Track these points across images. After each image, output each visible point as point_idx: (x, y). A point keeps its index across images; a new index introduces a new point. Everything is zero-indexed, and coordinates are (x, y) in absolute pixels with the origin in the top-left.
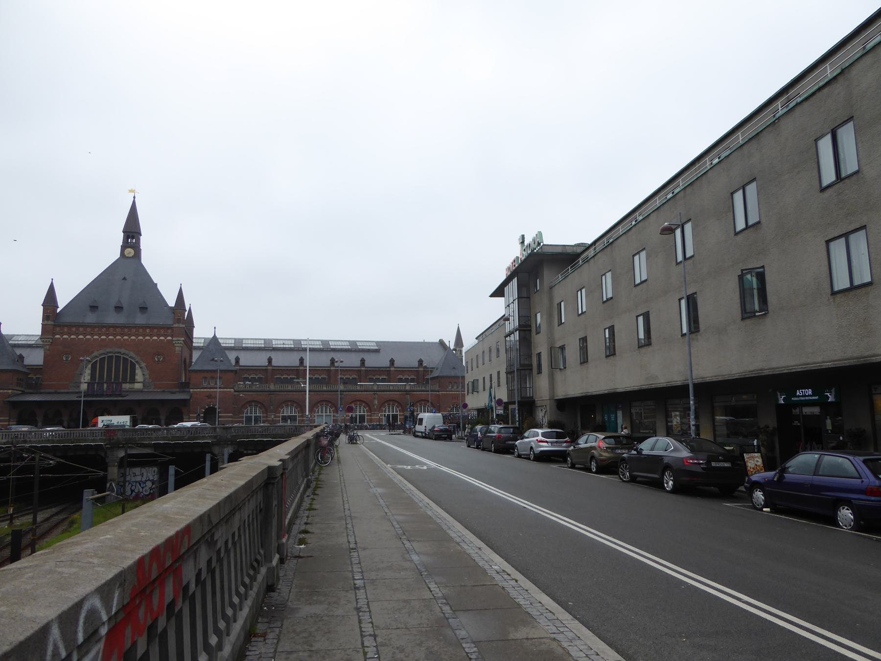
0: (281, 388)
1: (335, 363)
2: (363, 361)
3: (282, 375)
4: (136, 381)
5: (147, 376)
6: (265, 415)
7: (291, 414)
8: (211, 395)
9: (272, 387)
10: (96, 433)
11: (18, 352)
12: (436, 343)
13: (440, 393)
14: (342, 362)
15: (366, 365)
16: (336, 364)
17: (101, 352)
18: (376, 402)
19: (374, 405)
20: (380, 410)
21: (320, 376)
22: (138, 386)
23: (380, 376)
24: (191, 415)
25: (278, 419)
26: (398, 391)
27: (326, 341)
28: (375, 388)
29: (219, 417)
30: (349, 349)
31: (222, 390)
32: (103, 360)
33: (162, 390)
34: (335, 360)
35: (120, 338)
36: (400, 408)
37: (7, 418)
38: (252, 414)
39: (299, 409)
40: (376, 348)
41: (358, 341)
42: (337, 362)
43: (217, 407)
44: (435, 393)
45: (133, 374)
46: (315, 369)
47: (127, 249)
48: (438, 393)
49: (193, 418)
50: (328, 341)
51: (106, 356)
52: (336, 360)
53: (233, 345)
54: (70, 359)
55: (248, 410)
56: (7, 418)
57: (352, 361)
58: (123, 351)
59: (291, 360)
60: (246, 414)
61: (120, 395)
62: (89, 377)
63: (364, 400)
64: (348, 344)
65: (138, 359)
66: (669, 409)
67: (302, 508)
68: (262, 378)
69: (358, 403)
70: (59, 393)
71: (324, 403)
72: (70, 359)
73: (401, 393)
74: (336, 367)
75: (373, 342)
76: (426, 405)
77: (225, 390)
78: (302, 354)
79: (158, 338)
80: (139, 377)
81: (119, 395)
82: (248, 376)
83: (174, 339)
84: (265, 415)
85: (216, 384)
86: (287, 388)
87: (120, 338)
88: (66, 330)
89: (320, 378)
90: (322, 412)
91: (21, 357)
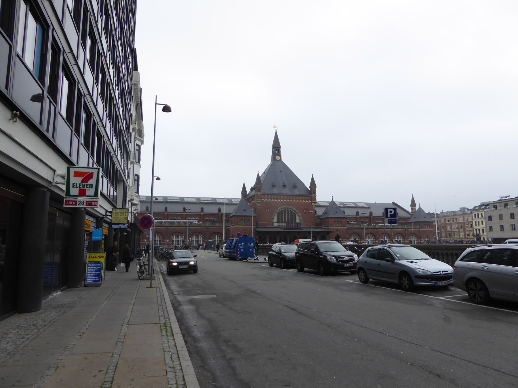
1: (186, 211)
2: (202, 210)
5: (302, 220)
9: (406, 227)
11: (342, 210)
12: (390, 204)
13: (420, 230)
14: (190, 210)
15: (204, 212)
16: (186, 211)
17: (282, 207)
23: (379, 221)
26: (401, 229)
27: (214, 198)
28: (391, 227)
30: (195, 202)
34: (185, 208)
35: (276, 200)
36: (374, 237)
38: (177, 240)
41: (217, 198)
42: (187, 209)
44: (418, 230)
46: (212, 215)
48: (419, 230)
50: (167, 197)
51: (280, 211)
52: (187, 208)
53: (145, 200)
54: (268, 211)
58: (291, 207)
59: (214, 210)
61: (300, 229)
62: (277, 220)
64: (195, 199)
65: (297, 211)
69: (214, 235)
70: (266, 227)
72: (268, 211)
73: (403, 229)
74: (186, 213)
75: (210, 198)
78: (219, 206)
79: (284, 200)
83: (313, 202)
88: (266, 197)
89: (209, 219)
90: (176, 239)
91: (344, 212)
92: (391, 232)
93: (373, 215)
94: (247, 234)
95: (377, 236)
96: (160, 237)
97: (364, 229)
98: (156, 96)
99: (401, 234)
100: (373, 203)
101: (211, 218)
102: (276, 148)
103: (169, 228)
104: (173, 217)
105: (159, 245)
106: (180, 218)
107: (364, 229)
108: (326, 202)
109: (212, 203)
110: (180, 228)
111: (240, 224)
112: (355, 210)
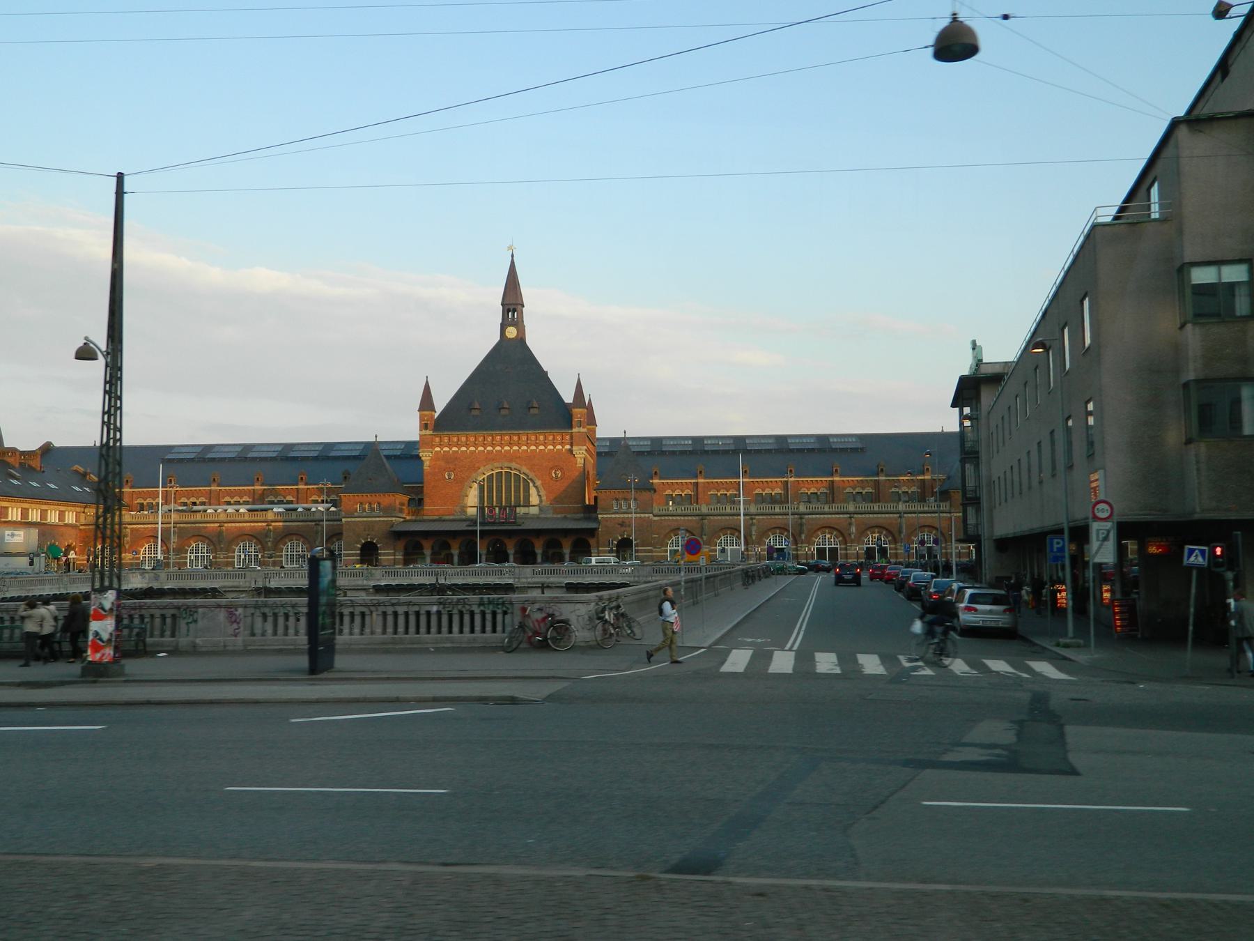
0: (837, 509)
4: (531, 504)
5: (544, 498)
6: (843, 546)
7: (781, 547)
8: (623, 522)
18: (853, 529)
19: (850, 535)
20: (859, 540)
21: (154, 500)
22: (534, 511)
24: (600, 549)
29: (637, 551)
31: (638, 515)
32: (491, 477)
33: (563, 515)
37: (392, 551)
40: (859, 445)
43: (633, 537)
45: (527, 496)
47: (509, 328)
48: (948, 515)
49: (605, 552)
55: (721, 540)
56: (392, 551)
60: (817, 545)
61: (514, 523)
63: (836, 527)
66: (358, 552)
69: (729, 532)
71: (778, 531)
76: (931, 533)
77: (642, 515)
80: (534, 499)
81: (514, 523)
84: (843, 546)
85: (629, 507)
86: (216, 519)
87: (517, 448)
92: (850, 524)
94: (361, 541)
95: (800, 536)
96: (836, 540)
98: (120, 177)
99: (887, 529)
102: (512, 303)
104: (232, 498)
108: (121, 458)
109: (820, 451)
111: (356, 514)
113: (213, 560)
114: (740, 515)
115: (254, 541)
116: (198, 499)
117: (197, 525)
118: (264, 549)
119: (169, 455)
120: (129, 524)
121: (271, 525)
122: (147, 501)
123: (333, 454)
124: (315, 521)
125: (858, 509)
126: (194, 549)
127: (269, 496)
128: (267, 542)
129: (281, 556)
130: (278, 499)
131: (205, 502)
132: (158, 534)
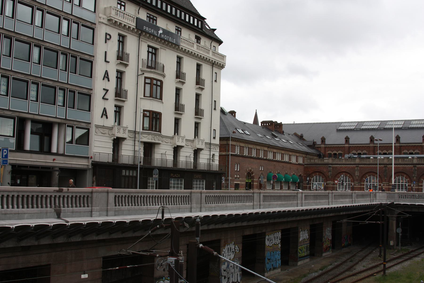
3: (332, 151)
10: (409, 195)
15: (350, 142)
16: (375, 142)
25: (363, 186)
34: (374, 138)
39: (408, 179)
55: (314, 178)
57: (339, 139)
67: (404, 260)
68: (342, 153)
82: (331, 152)
86: (382, 162)
93: (327, 142)
97: (378, 166)
98: (106, 52)
100: (290, 124)
101: (335, 152)
103: (388, 166)
104: (408, 150)
105: (404, 191)
106: (418, 152)
107: (378, 166)
110: (403, 166)
112: (344, 135)
113: (326, 186)
114: (392, 164)
115: (405, 176)
116: (357, 151)
117: (370, 166)
118: (411, 181)
119: (363, 126)
120: (331, 164)
121: (416, 167)
122: (334, 152)
123: (363, 127)
124: (384, 164)
125: (374, 162)
126: (315, 179)
127: (404, 150)
128: (413, 177)
129: (364, 185)
130: (389, 152)
131: (366, 153)
132: (377, 172)
